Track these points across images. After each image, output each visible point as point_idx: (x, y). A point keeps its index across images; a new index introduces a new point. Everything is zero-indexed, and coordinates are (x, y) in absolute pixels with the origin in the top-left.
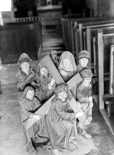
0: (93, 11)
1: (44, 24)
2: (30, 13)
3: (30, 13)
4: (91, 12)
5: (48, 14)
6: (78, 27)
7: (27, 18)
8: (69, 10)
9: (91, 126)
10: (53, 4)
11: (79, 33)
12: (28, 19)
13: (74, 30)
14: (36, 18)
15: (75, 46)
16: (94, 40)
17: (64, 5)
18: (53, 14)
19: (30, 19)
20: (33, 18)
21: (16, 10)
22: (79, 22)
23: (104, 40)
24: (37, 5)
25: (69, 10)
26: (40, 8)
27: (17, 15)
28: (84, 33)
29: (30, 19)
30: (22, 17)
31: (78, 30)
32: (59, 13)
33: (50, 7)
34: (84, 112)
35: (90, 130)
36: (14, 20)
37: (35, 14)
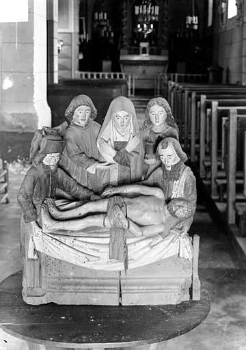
0: (228, 71)
1: (132, 86)
2: (107, 64)
3: (107, 64)
4: (224, 74)
5: (140, 69)
6: (209, 105)
7: (101, 74)
8: (181, 65)
9: (237, 303)
10: (151, 53)
11: (210, 117)
12: (103, 76)
13: (198, 109)
14: (118, 74)
15: (198, 132)
16: (190, 100)
17: (170, 55)
18: (151, 70)
19: (106, 75)
20: (112, 74)
21: (81, 57)
22: (212, 95)
23: (238, 122)
24: (121, 51)
25: (181, 65)
26: (122, 58)
27: (82, 66)
28: (199, 103)
29: (106, 75)
30: (93, 70)
31: (209, 110)
32: (160, 69)
33: (145, 57)
34: (146, 108)
35: (235, 310)
36: (76, 74)
37: (116, 67)
